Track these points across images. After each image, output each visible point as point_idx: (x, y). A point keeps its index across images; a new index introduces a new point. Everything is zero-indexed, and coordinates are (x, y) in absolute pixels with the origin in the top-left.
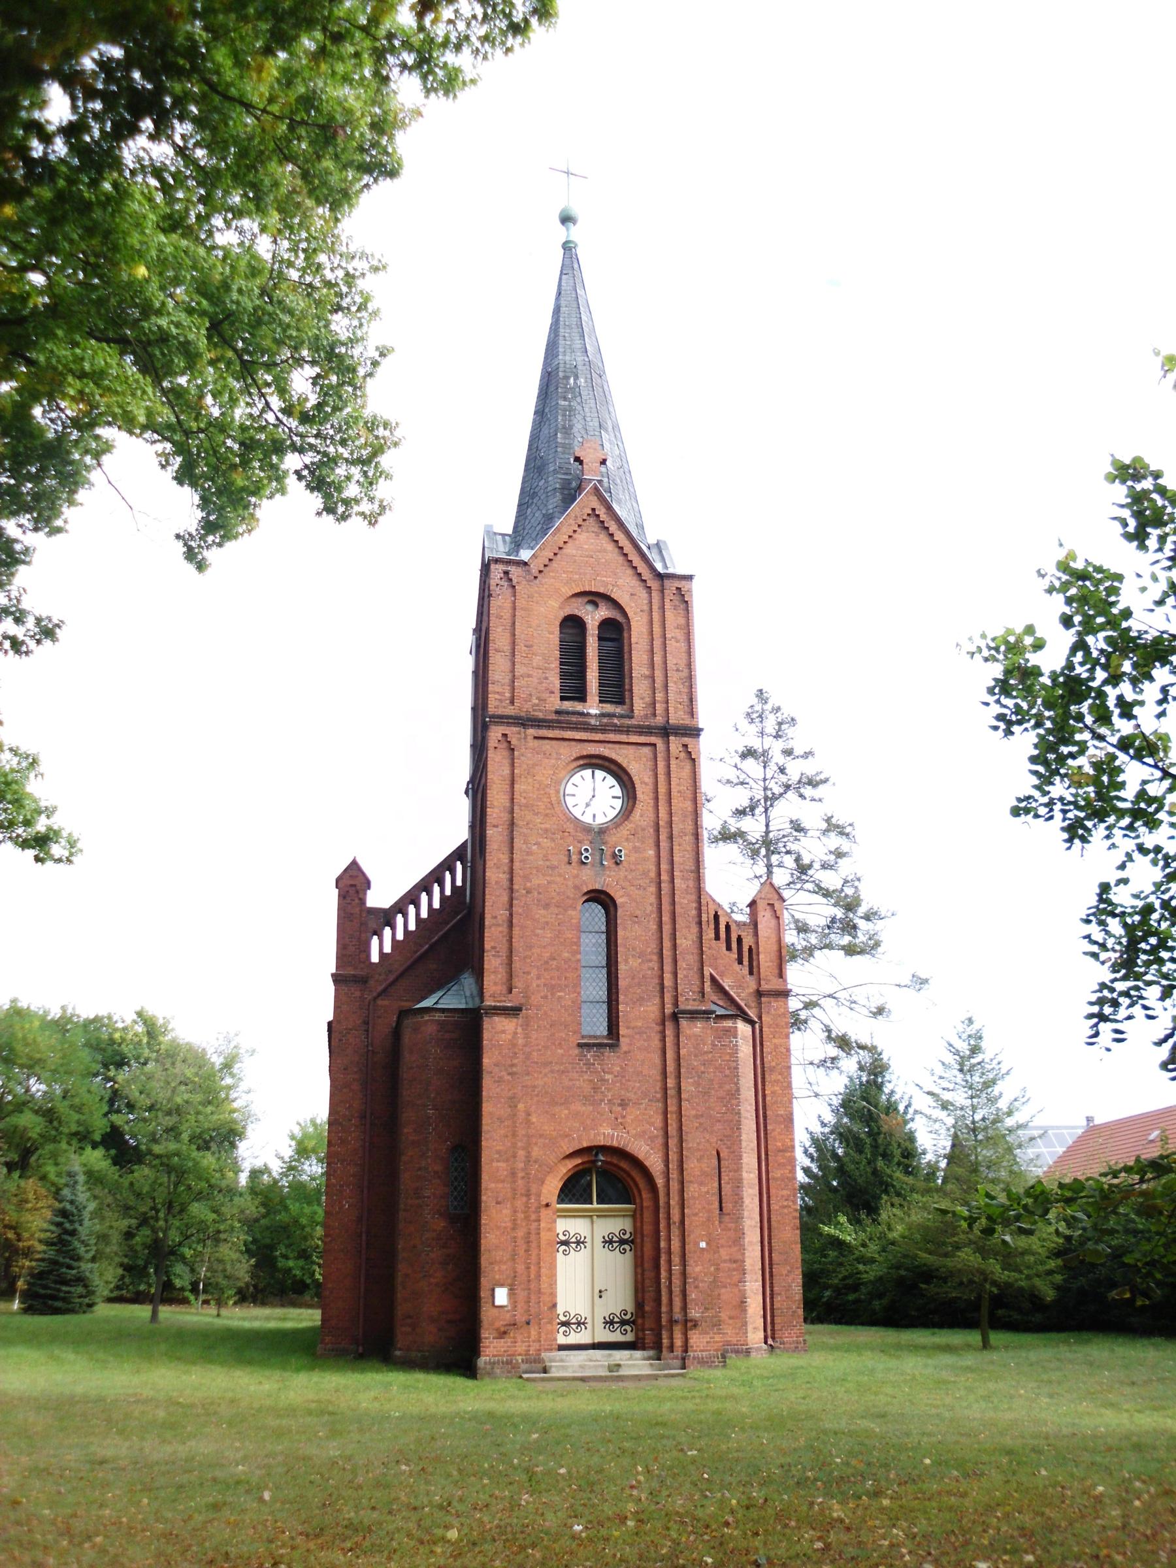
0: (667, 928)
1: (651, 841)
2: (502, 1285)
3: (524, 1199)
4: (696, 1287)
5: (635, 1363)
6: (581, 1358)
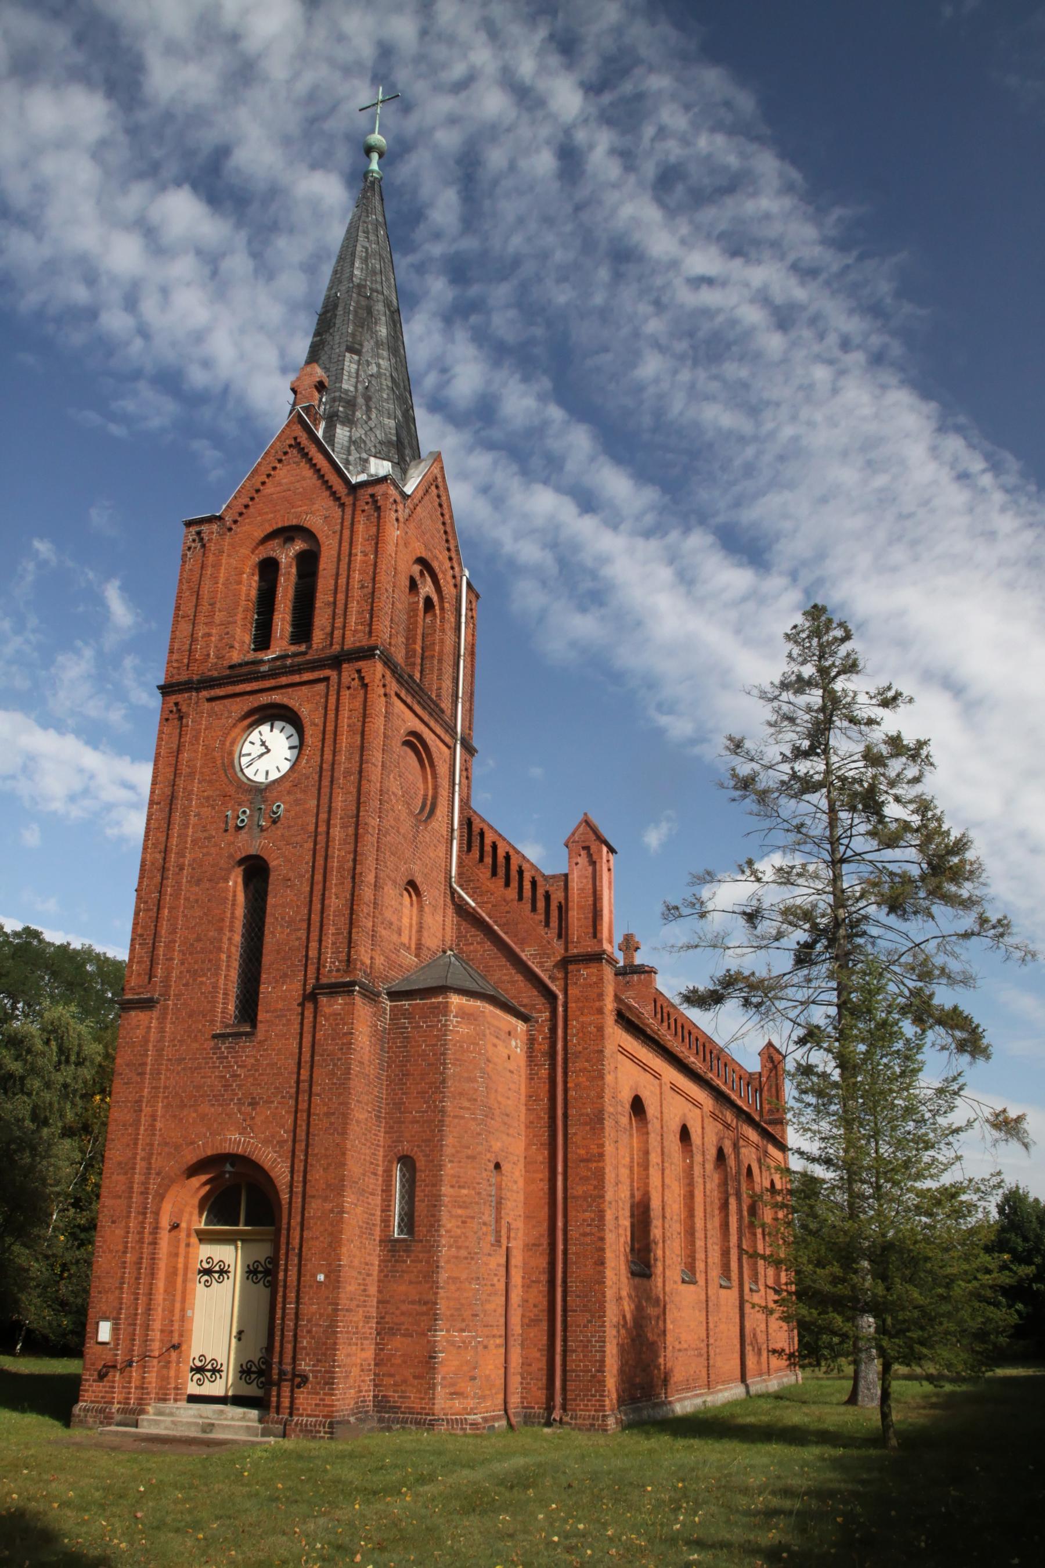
0: (318, 888)
2: (106, 1319)
3: (141, 1218)
4: (309, 1332)
6: (192, 1412)
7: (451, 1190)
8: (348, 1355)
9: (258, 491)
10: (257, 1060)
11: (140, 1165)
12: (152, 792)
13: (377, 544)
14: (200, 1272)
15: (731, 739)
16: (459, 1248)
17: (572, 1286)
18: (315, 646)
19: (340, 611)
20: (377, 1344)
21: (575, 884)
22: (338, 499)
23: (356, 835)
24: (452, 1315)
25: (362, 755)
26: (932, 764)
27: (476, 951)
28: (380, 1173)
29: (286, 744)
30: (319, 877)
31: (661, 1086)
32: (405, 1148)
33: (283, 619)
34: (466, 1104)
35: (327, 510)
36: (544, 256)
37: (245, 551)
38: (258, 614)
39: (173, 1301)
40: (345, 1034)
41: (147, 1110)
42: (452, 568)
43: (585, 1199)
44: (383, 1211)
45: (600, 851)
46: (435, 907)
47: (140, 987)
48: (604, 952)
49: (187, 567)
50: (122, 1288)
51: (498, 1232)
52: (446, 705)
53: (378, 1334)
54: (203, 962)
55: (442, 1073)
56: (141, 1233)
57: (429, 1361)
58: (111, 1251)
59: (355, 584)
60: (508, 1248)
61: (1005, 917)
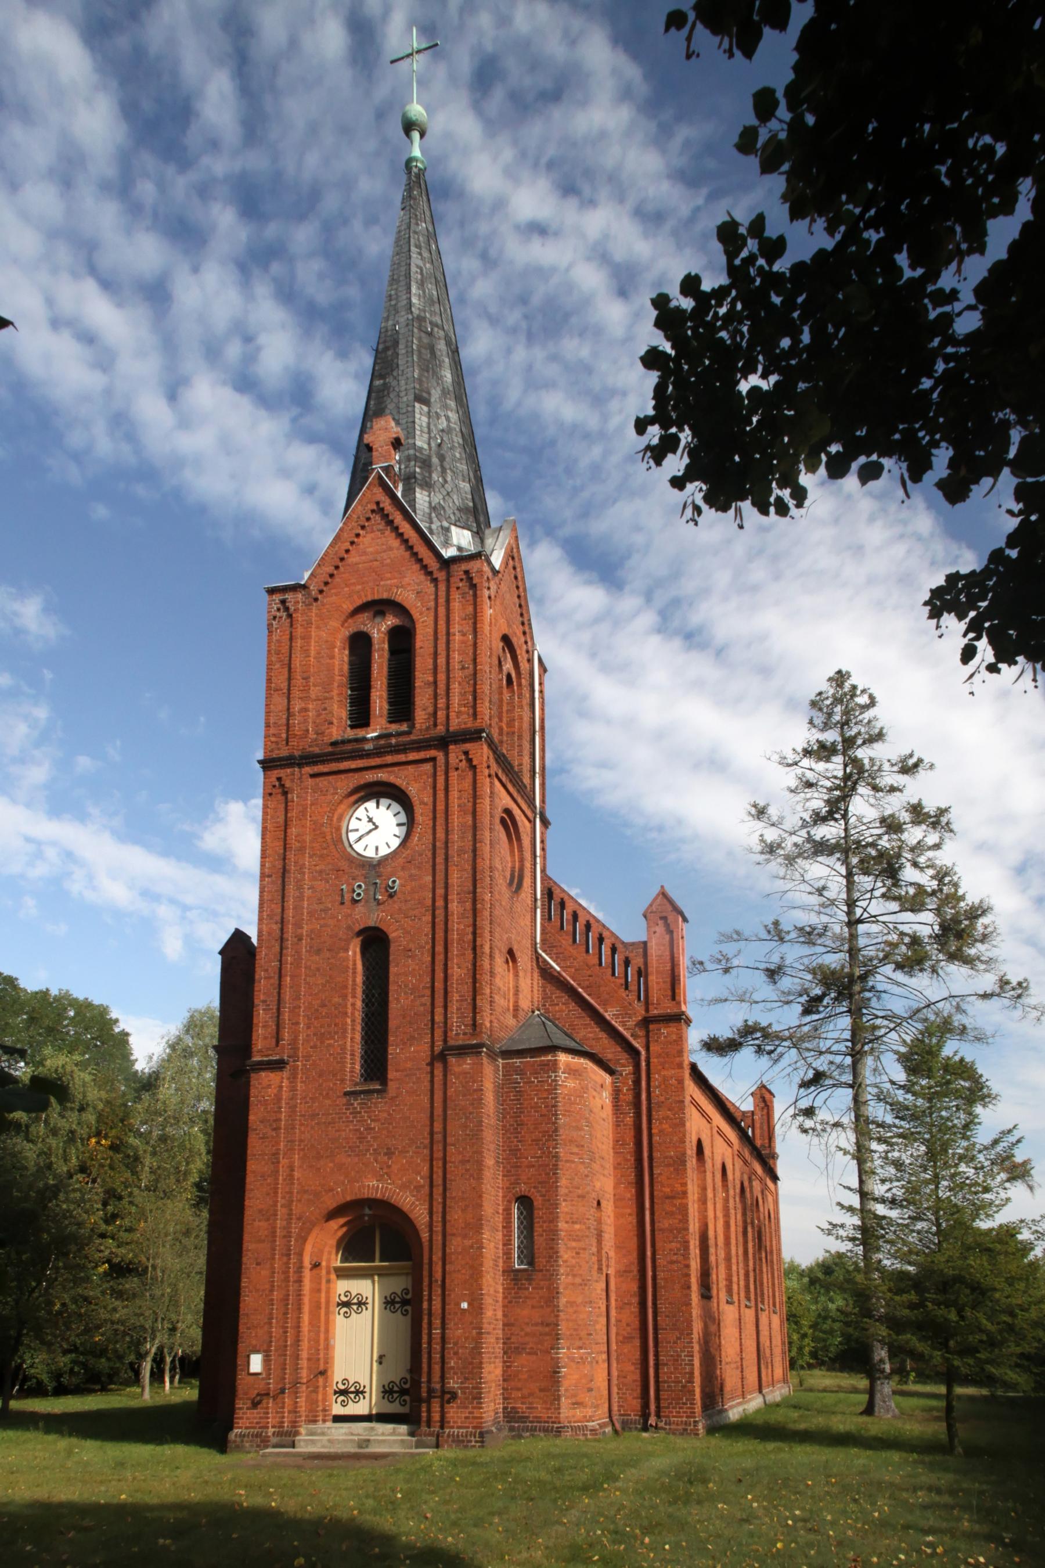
0: (439, 958)
1: (429, 866)
2: (257, 1352)
3: (285, 1259)
5: (391, 1437)
6: (343, 1431)
7: (566, 1225)
8: (490, 1373)
9: (342, 559)
10: (389, 1114)
11: (281, 1212)
12: (263, 865)
13: (475, 623)
14: (338, 1304)
15: (755, 806)
16: (574, 1276)
17: (662, 1307)
18: (417, 726)
19: (441, 691)
20: (504, 1362)
21: (653, 951)
22: (430, 573)
23: (475, 910)
24: (571, 1335)
25: (475, 835)
26: (951, 831)
27: (561, 1011)
28: (501, 1211)
29: (394, 821)
30: (440, 948)
31: (711, 1128)
32: (523, 1189)
33: (381, 697)
34: (575, 1150)
35: (418, 584)
36: (347, 184)
37: (334, 624)
38: (352, 689)
39: (318, 1333)
40: (475, 1090)
41: (284, 1162)
42: (526, 642)
43: (671, 1231)
44: (504, 1245)
45: (677, 921)
46: (525, 971)
47: (268, 1049)
48: (683, 1013)
49: (274, 638)
50: (271, 1323)
51: (600, 1261)
52: (526, 780)
53: (505, 1353)
54: (329, 1026)
55: (555, 1123)
56: (286, 1272)
57: (553, 1376)
58: (257, 1290)
59: (455, 664)
60: (607, 1275)
61: (1026, 980)
